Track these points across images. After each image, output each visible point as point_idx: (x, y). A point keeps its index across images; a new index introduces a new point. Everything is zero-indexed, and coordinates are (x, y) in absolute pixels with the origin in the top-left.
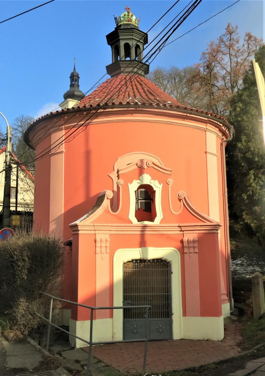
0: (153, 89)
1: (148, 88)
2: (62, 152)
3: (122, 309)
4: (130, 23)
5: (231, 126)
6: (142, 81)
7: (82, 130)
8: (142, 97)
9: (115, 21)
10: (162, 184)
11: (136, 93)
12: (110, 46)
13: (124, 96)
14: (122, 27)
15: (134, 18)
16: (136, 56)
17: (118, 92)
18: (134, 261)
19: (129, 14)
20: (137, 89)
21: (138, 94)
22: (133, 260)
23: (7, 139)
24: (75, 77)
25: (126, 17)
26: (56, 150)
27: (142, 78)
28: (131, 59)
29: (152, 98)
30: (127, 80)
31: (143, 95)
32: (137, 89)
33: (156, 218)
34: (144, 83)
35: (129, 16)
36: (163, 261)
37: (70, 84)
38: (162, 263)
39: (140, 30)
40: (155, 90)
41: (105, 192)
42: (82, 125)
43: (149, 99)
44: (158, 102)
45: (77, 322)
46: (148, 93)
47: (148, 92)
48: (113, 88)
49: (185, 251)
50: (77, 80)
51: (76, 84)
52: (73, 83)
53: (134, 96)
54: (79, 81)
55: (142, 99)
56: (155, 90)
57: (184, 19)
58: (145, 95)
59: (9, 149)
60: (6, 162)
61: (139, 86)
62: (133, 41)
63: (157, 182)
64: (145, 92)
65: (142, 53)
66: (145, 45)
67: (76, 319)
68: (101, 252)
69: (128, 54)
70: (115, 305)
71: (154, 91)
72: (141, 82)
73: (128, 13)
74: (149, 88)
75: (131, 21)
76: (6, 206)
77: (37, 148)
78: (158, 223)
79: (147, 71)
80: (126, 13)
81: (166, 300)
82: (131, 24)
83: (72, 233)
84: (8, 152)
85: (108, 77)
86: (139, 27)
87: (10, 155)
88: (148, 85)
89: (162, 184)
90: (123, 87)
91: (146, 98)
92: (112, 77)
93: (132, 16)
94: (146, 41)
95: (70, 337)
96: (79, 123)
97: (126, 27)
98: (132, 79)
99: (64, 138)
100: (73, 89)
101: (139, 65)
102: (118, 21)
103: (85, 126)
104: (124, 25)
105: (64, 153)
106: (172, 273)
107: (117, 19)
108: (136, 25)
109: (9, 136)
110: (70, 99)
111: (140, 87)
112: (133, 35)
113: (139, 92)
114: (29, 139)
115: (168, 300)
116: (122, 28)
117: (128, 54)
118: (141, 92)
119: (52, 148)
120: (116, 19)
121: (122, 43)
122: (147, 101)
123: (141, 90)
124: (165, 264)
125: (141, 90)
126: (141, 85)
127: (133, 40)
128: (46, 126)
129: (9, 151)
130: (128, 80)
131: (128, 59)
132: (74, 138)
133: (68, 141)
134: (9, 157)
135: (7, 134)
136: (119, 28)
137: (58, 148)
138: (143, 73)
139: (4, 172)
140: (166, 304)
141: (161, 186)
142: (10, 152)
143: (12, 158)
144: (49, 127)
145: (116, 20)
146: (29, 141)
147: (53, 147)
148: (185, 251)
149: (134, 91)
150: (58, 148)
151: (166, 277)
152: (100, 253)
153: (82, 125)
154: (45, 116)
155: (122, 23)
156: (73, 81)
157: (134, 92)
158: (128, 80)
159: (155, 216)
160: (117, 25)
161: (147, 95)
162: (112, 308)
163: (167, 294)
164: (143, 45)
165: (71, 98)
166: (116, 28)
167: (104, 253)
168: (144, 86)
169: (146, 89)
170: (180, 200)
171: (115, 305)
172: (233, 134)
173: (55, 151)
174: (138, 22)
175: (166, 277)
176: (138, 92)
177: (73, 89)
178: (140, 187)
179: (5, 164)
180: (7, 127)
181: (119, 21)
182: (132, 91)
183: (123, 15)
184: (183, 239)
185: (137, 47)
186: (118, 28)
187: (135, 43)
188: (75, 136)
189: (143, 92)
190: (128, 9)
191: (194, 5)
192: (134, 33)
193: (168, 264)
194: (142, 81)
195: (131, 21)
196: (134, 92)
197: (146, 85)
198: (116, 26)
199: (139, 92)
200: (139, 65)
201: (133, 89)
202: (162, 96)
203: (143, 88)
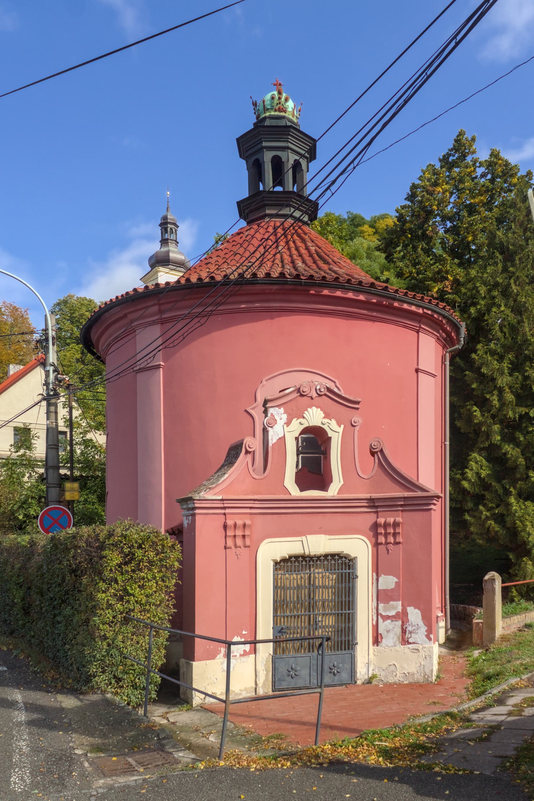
0: (325, 250)
1: (317, 248)
2: (158, 367)
3: (272, 644)
4: (282, 114)
5: (461, 323)
6: (305, 234)
7: (199, 324)
8: (306, 264)
9: (254, 109)
10: (342, 426)
11: (295, 257)
12: (244, 162)
13: (273, 261)
14: (267, 123)
15: (290, 105)
16: (294, 182)
17: (260, 259)
18: (293, 559)
19: (281, 96)
20: (297, 249)
21: (299, 258)
22: (290, 557)
23: (47, 339)
24: (169, 225)
25: (276, 101)
26: (149, 361)
27: (305, 228)
28: (284, 189)
29: (325, 267)
30: (278, 237)
31: (308, 261)
32: (297, 249)
33: (332, 485)
34: (309, 237)
35: (280, 101)
36: (341, 558)
37: (160, 239)
38: (340, 561)
39: (301, 129)
40: (329, 252)
41: (243, 440)
42: (199, 314)
43: (320, 269)
44: (336, 276)
45: (194, 663)
46: (317, 258)
47: (318, 255)
48: (245, 258)
49: (379, 541)
50: (174, 231)
51: (172, 238)
52: (166, 236)
53: (291, 263)
54: (178, 232)
55: (307, 268)
56: (329, 252)
57: (406, 102)
58: (312, 261)
59: (53, 359)
60: (46, 384)
61: (299, 243)
62: (290, 153)
63: (333, 422)
64: (311, 255)
65: (305, 188)
66: (310, 162)
67: (193, 660)
68: (236, 546)
69: (278, 179)
70: (260, 636)
71: (328, 253)
72: (303, 235)
73: (280, 93)
74: (319, 248)
75: (285, 111)
76: (51, 465)
77: (108, 359)
78: (336, 494)
79: (313, 217)
80: (276, 93)
81: (345, 622)
82: (284, 117)
83: (183, 513)
84: (51, 365)
85: (243, 223)
86: (299, 123)
87: (54, 371)
88: (316, 242)
89: (342, 426)
90: (269, 251)
91: (314, 266)
92: (248, 223)
93: (286, 100)
94: (312, 155)
95: (182, 690)
96: (193, 311)
97: (274, 123)
98: (289, 237)
99: (160, 341)
100: (164, 249)
101: (305, 208)
102: (258, 110)
103: (204, 316)
104: (272, 118)
105: (161, 369)
106: (357, 577)
107: (258, 104)
108: (295, 120)
109: (51, 333)
110: (161, 269)
111: (303, 245)
112: (289, 140)
113: (300, 255)
114: (92, 339)
115: (349, 622)
116: (268, 125)
117: (278, 179)
118: (304, 256)
119: (160, 338)
120: (255, 104)
121: (268, 156)
122: (317, 273)
123: (303, 251)
124: (345, 563)
125: (303, 251)
126: (303, 241)
127: (289, 151)
128: (125, 316)
129: (53, 363)
130: (281, 236)
131: (279, 189)
132: (184, 338)
133: (171, 345)
134: (52, 376)
135: (46, 330)
136: (262, 124)
137: (152, 358)
138: (306, 219)
139: (44, 403)
140: (345, 628)
141: (341, 430)
142: (53, 365)
143: (59, 376)
144: (131, 317)
145: (256, 106)
146: (92, 345)
147: (140, 358)
148: (379, 541)
149: (290, 252)
150: (152, 358)
151: (347, 584)
152: (233, 547)
153: (199, 314)
154: (122, 296)
155: (267, 114)
156: (166, 232)
157: (291, 256)
158: (281, 236)
159: (330, 480)
160: (258, 117)
161: (315, 262)
162: (254, 642)
163: (347, 611)
164: (307, 162)
165: (163, 266)
166: (255, 124)
167: (240, 547)
168: (309, 244)
169: (313, 249)
170: (373, 454)
171: (260, 636)
172: (464, 338)
173: (146, 363)
174: (298, 113)
175: (347, 584)
176: (298, 255)
177: (164, 249)
178: (304, 432)
179: (45, 388)
180: (46, 316)
181: (261, 110)
182: (288, 253)
183: (268, 97)
184: (376, 521)
185: (297, 166)
186: (259, 124)
187: (293, 158)
188: (185, 336)
189: (308, 255)
190: (280, 84)
191: (426, 73)
192: (289, 137)
193: (351, 563)
194: (305, 234)
195: (285, 111)
196: (291, 256)
197: (313, 242)
198: (256, 121)
199: (300, 255)
200: (305, 208)
201: (289, 249)
202: (342, 265)
203: (307, 248)
